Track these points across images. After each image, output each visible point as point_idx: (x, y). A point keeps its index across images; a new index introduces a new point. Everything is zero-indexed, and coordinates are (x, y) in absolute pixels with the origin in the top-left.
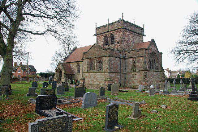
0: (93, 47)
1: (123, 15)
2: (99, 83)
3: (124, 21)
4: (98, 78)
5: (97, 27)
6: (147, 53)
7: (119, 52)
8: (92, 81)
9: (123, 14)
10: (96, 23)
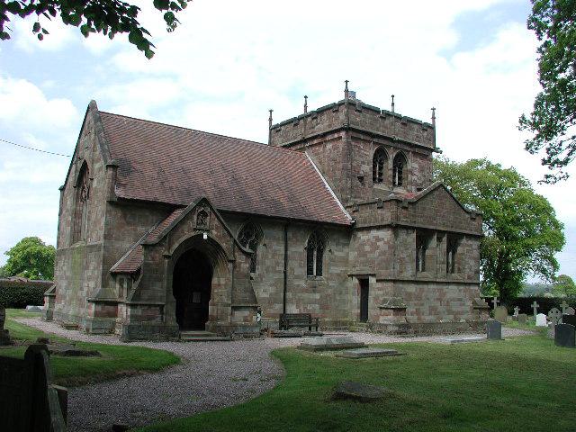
0: (436, 193)
1: (434, 114)
2: (455, 318)
3: (398, 117)
4: (453, 300)
5: (274, 123)
6: (310, 329)
7: (472, 219)
8: (433, 310)
9: (433, 109)
10: (271, 111)
